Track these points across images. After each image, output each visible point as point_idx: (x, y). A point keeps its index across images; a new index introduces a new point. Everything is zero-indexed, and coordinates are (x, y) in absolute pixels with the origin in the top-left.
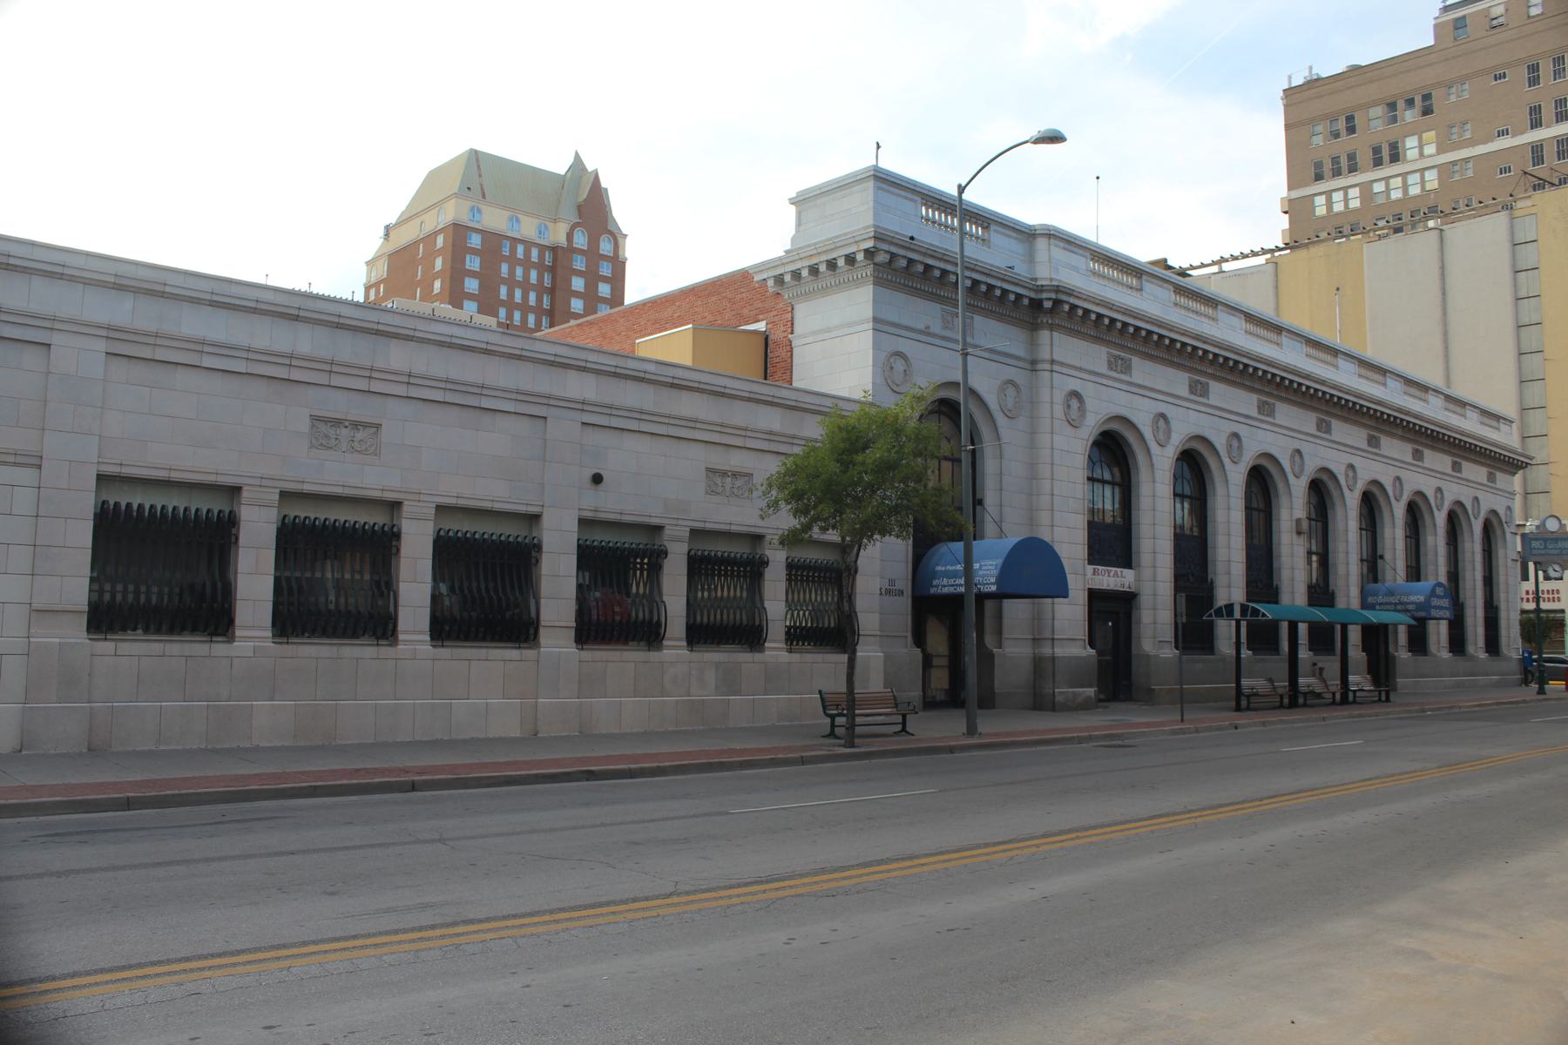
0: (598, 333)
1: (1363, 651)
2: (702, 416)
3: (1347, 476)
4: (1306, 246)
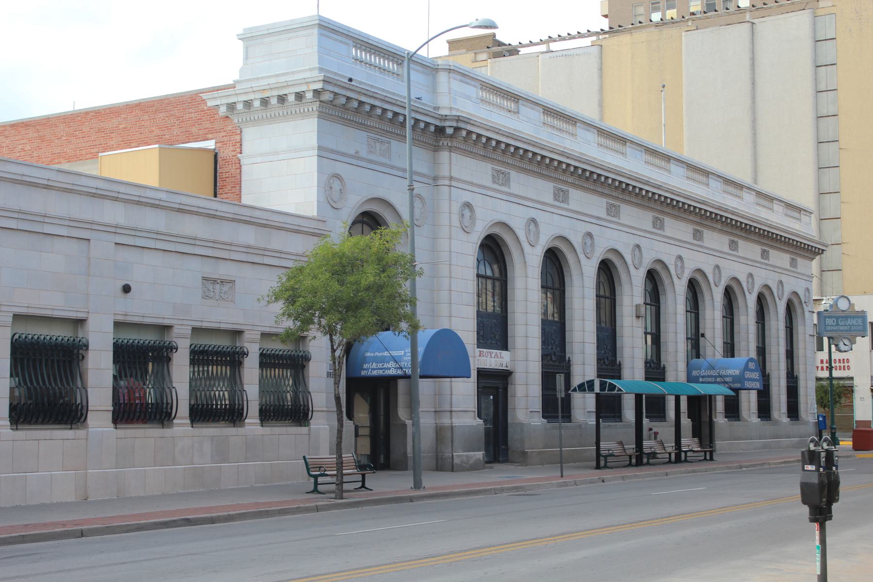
0: (35, 135)
1: (688, 418)
2: (200, 235)
3: (676, 266)
4: (629, 31)
